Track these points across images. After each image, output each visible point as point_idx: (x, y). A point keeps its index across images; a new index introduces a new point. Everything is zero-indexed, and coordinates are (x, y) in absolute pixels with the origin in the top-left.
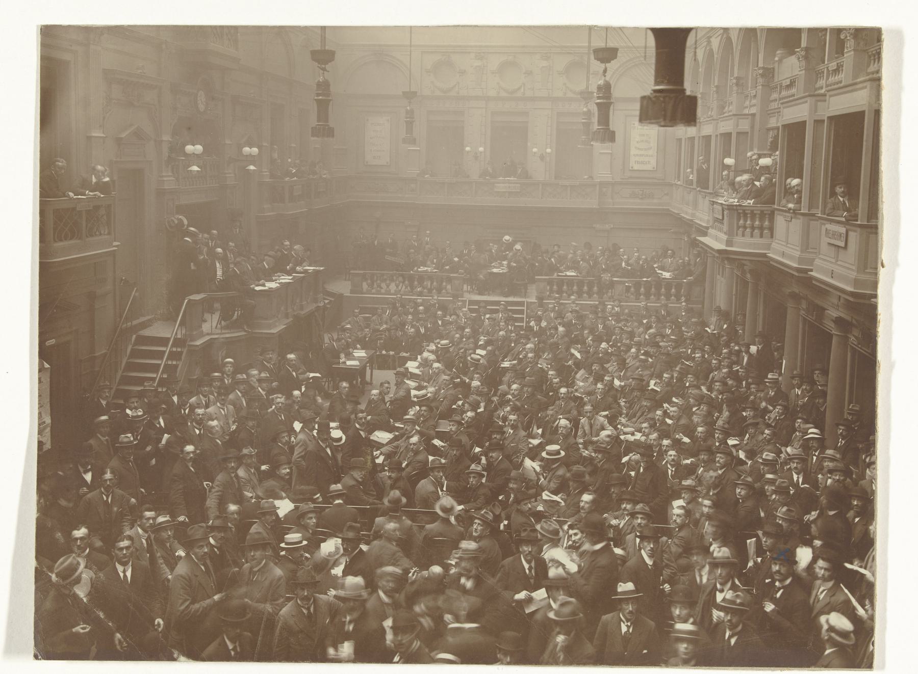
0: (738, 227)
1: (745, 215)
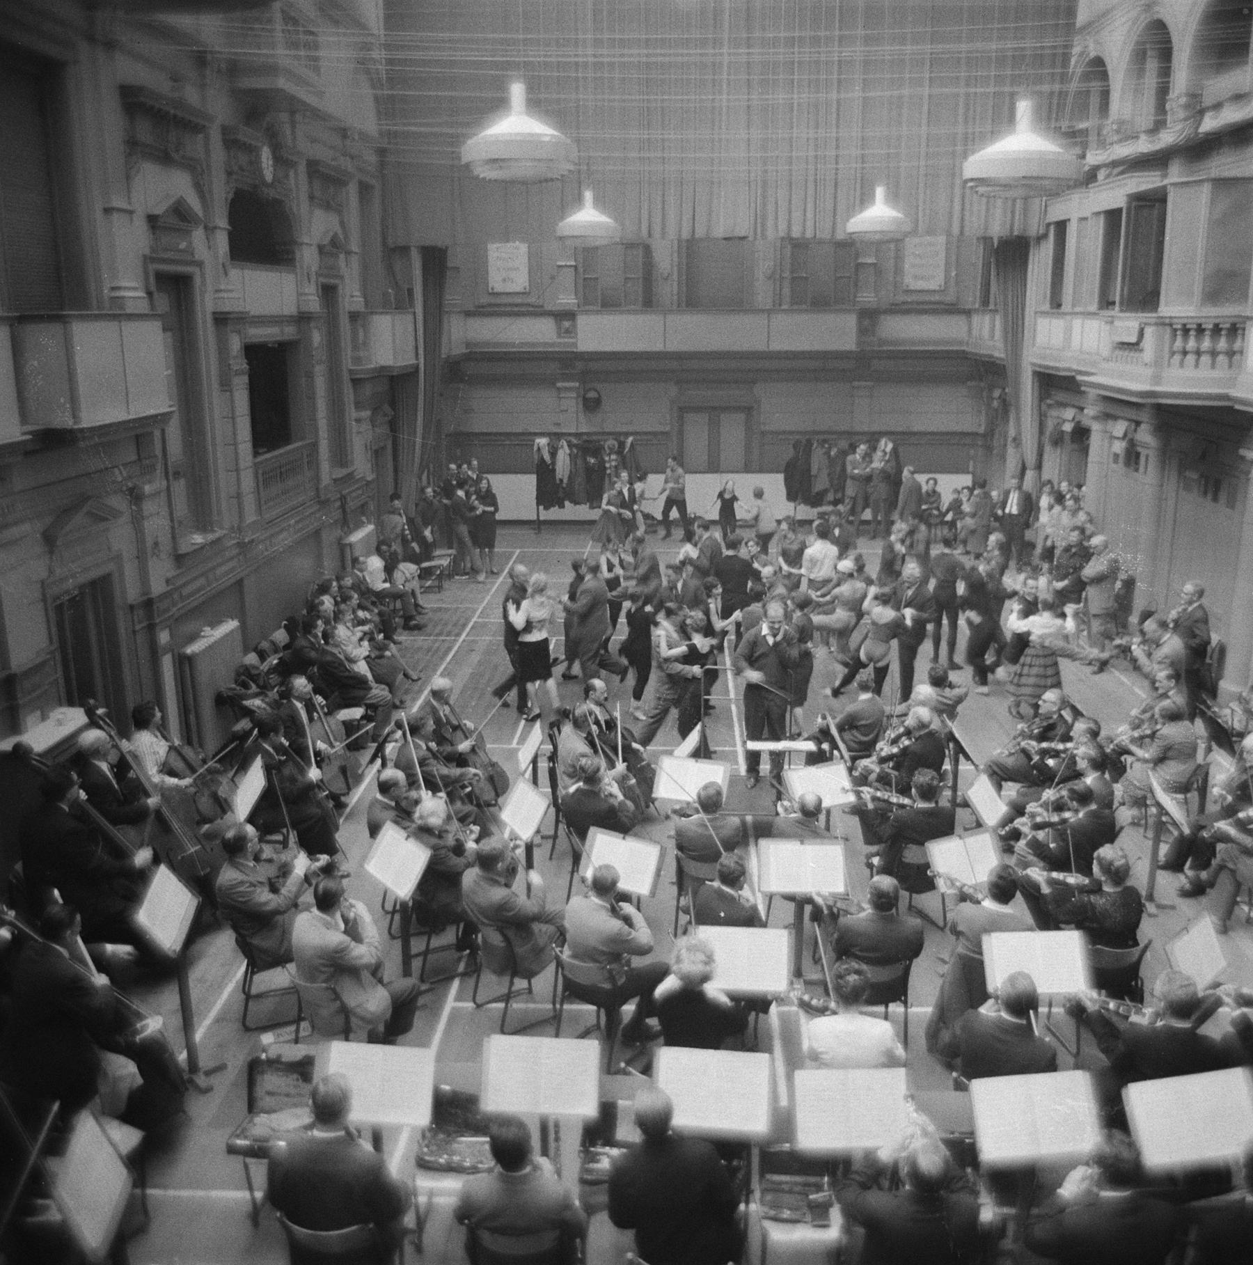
0: (1173, 353)
1: (1186, 331)
